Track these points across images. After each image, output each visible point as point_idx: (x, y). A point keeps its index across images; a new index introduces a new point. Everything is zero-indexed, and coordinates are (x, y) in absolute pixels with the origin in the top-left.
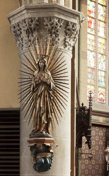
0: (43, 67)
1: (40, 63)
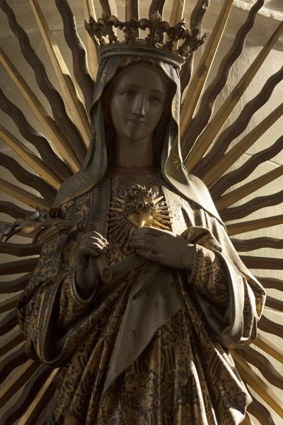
0: (144, 133)
1: (117, 101)
